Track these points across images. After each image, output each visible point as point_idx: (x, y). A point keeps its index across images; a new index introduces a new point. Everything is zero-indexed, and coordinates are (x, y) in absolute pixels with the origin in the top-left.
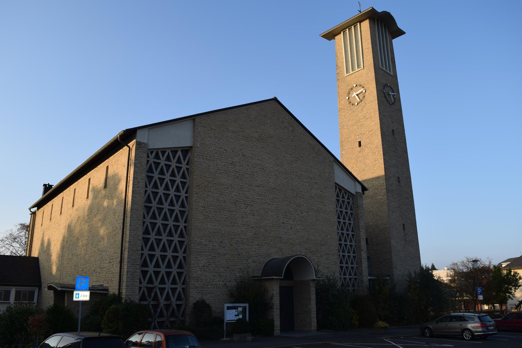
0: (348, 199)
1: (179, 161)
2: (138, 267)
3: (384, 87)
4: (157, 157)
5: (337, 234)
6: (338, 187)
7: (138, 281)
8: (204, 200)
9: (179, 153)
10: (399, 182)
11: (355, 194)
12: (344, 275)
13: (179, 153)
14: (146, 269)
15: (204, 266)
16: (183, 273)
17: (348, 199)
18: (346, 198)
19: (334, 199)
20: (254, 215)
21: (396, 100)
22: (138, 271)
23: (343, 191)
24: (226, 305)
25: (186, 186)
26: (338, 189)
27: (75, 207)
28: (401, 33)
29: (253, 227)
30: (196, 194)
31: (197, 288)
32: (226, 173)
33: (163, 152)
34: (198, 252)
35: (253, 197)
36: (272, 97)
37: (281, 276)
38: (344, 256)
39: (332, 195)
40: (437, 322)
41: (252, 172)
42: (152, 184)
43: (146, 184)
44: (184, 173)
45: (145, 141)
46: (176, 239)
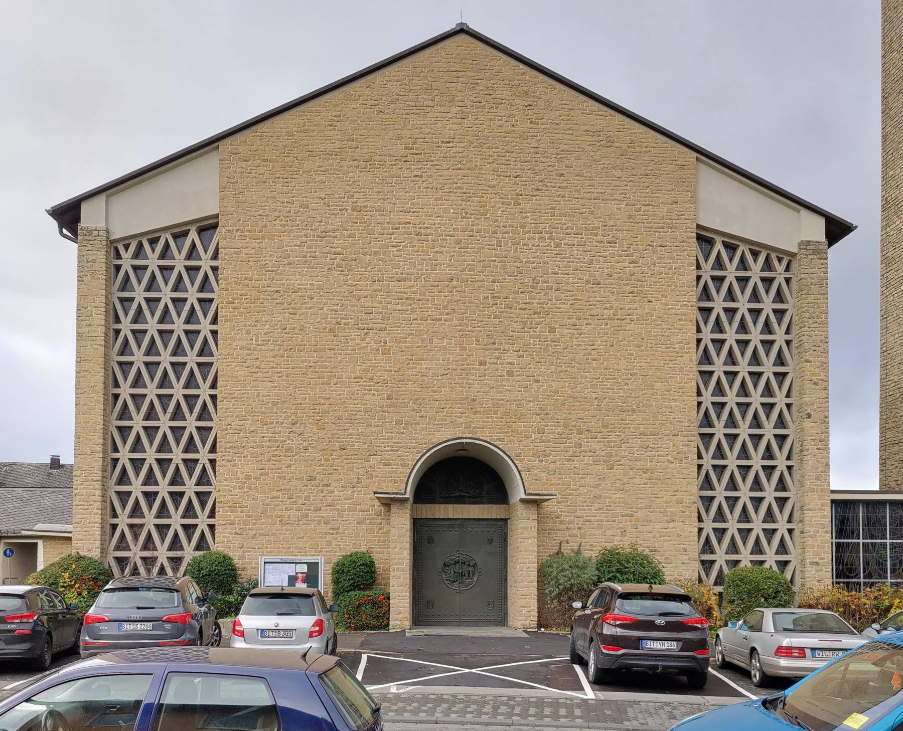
8: (248, 333)
9: (193, 235)
13: (193, 235)
14: (709, 493)
15: (248, 477)
20: (386, 352)
23: (743, 248)
29: (385, 382)
30: (226, 321)
39: (682, 264)
42: (711, 323)
46: (191, 423)
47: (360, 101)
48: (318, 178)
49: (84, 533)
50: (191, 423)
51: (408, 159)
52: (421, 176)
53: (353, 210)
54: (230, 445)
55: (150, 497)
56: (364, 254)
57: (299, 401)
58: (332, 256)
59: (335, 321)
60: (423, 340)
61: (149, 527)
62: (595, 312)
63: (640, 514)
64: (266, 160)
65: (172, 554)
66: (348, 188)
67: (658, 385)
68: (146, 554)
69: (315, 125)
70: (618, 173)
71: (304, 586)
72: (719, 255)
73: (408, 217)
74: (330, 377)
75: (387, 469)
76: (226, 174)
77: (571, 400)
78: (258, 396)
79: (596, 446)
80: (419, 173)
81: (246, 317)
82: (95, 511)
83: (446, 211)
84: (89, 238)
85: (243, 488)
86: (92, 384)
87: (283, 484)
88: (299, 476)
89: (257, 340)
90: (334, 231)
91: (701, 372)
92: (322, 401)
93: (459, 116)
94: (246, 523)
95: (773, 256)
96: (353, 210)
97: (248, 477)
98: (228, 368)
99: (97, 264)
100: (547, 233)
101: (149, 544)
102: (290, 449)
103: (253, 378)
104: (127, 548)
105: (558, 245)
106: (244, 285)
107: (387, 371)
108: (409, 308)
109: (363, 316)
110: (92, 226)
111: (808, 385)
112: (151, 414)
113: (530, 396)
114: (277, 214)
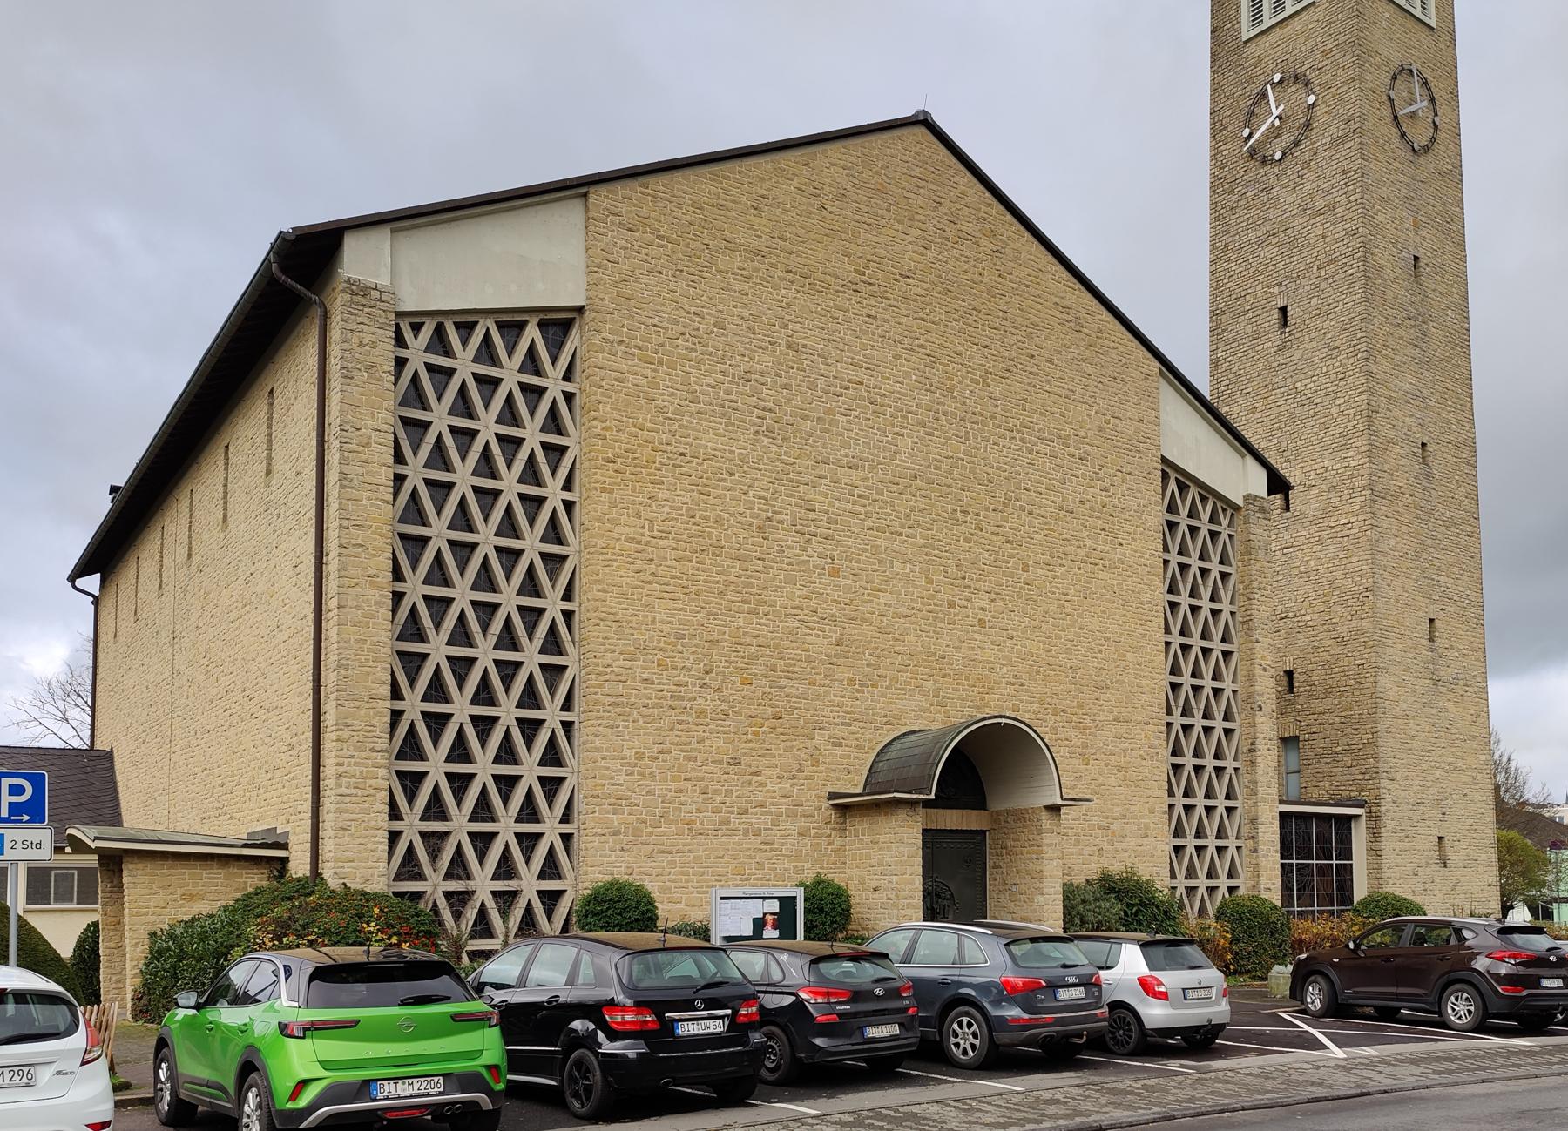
0: (1213, 519)
1: (532, 363)
2: (381, 759)
3: (1394, 78)
4: (440, 343)
5: (1162, 647)
6: (1173, 475)
7: (386, 808)
9: (532, 333)
10: (1425, 462)
11: (1240, 502)
12: (1186, 795)
13: (532, 333)
15: (640, 756)
16: (561, 780)
17: (1211, 521)
18: (1205, 516)
19: (1158, 517)
20: (834, 573)
21: (1442, 135)
22: (382, 772)
23: (1193, 490)
25: (566, 463)
26: (1172, 485)
30: (603, 490)
31: (616, 833)
33: (466, 328)
36: (907, 112)
41: (828, 411)
43: (396, 441)
44: (553, 410)
45: (384, 281)
47: (795, 183)
49: (356, 848)
50: (531, 657)
51: (858, 287)
52: (875, 318)
53: (789, 347)
54: (611, 699)
55: (460, 783)
56: (805, 418)
57: (715, 636)
58: (761, 413)
59: (764, 515)
60: (880, 561)
61: (459, 837)
62: (1068, 549)
63: (1115, 826)
64: (660, 237)
65: (501, 886)
66: (780, 312)
67: (1130, 656)
68: (454, 886)
69: (734, 202)
70: (1088, 369)
71: (776, 934)
72: (532, 349)
73: (859, 375)
74: (759, 603)
75: (839, 751)
76: (601, 245)
77: (1045, 667)
78: (653, 622)
79: (1072, 733)
80: (873, 313)
81: (633, 489)
82: (378, 807)
83: (907, 376)
84: (364, 301)
85: (632, 774)
86: (371, 572)
87: (694, 770)
88: (718, 757)
89: (651, 529)
90: (763, 374)
91: (403, 537)
92: (748, 640)
93: (921, 242)
95: (1219, 505)
96: (789, 347)
97: (640, 756)
98: (607, 570)
100: (1019, 432)
101: (458, 867)
102: (702, 713)
103: (645, 592)
104: (420, 876)
105: (1030, 452)
106: (631, 434)
107: (834, 601)
108: (863, 510)
109: (803, 513)
110: (368, 279)
111: (1259, 671)
112: (461, 635)
113: (1004, 658)
114: (680, 328)
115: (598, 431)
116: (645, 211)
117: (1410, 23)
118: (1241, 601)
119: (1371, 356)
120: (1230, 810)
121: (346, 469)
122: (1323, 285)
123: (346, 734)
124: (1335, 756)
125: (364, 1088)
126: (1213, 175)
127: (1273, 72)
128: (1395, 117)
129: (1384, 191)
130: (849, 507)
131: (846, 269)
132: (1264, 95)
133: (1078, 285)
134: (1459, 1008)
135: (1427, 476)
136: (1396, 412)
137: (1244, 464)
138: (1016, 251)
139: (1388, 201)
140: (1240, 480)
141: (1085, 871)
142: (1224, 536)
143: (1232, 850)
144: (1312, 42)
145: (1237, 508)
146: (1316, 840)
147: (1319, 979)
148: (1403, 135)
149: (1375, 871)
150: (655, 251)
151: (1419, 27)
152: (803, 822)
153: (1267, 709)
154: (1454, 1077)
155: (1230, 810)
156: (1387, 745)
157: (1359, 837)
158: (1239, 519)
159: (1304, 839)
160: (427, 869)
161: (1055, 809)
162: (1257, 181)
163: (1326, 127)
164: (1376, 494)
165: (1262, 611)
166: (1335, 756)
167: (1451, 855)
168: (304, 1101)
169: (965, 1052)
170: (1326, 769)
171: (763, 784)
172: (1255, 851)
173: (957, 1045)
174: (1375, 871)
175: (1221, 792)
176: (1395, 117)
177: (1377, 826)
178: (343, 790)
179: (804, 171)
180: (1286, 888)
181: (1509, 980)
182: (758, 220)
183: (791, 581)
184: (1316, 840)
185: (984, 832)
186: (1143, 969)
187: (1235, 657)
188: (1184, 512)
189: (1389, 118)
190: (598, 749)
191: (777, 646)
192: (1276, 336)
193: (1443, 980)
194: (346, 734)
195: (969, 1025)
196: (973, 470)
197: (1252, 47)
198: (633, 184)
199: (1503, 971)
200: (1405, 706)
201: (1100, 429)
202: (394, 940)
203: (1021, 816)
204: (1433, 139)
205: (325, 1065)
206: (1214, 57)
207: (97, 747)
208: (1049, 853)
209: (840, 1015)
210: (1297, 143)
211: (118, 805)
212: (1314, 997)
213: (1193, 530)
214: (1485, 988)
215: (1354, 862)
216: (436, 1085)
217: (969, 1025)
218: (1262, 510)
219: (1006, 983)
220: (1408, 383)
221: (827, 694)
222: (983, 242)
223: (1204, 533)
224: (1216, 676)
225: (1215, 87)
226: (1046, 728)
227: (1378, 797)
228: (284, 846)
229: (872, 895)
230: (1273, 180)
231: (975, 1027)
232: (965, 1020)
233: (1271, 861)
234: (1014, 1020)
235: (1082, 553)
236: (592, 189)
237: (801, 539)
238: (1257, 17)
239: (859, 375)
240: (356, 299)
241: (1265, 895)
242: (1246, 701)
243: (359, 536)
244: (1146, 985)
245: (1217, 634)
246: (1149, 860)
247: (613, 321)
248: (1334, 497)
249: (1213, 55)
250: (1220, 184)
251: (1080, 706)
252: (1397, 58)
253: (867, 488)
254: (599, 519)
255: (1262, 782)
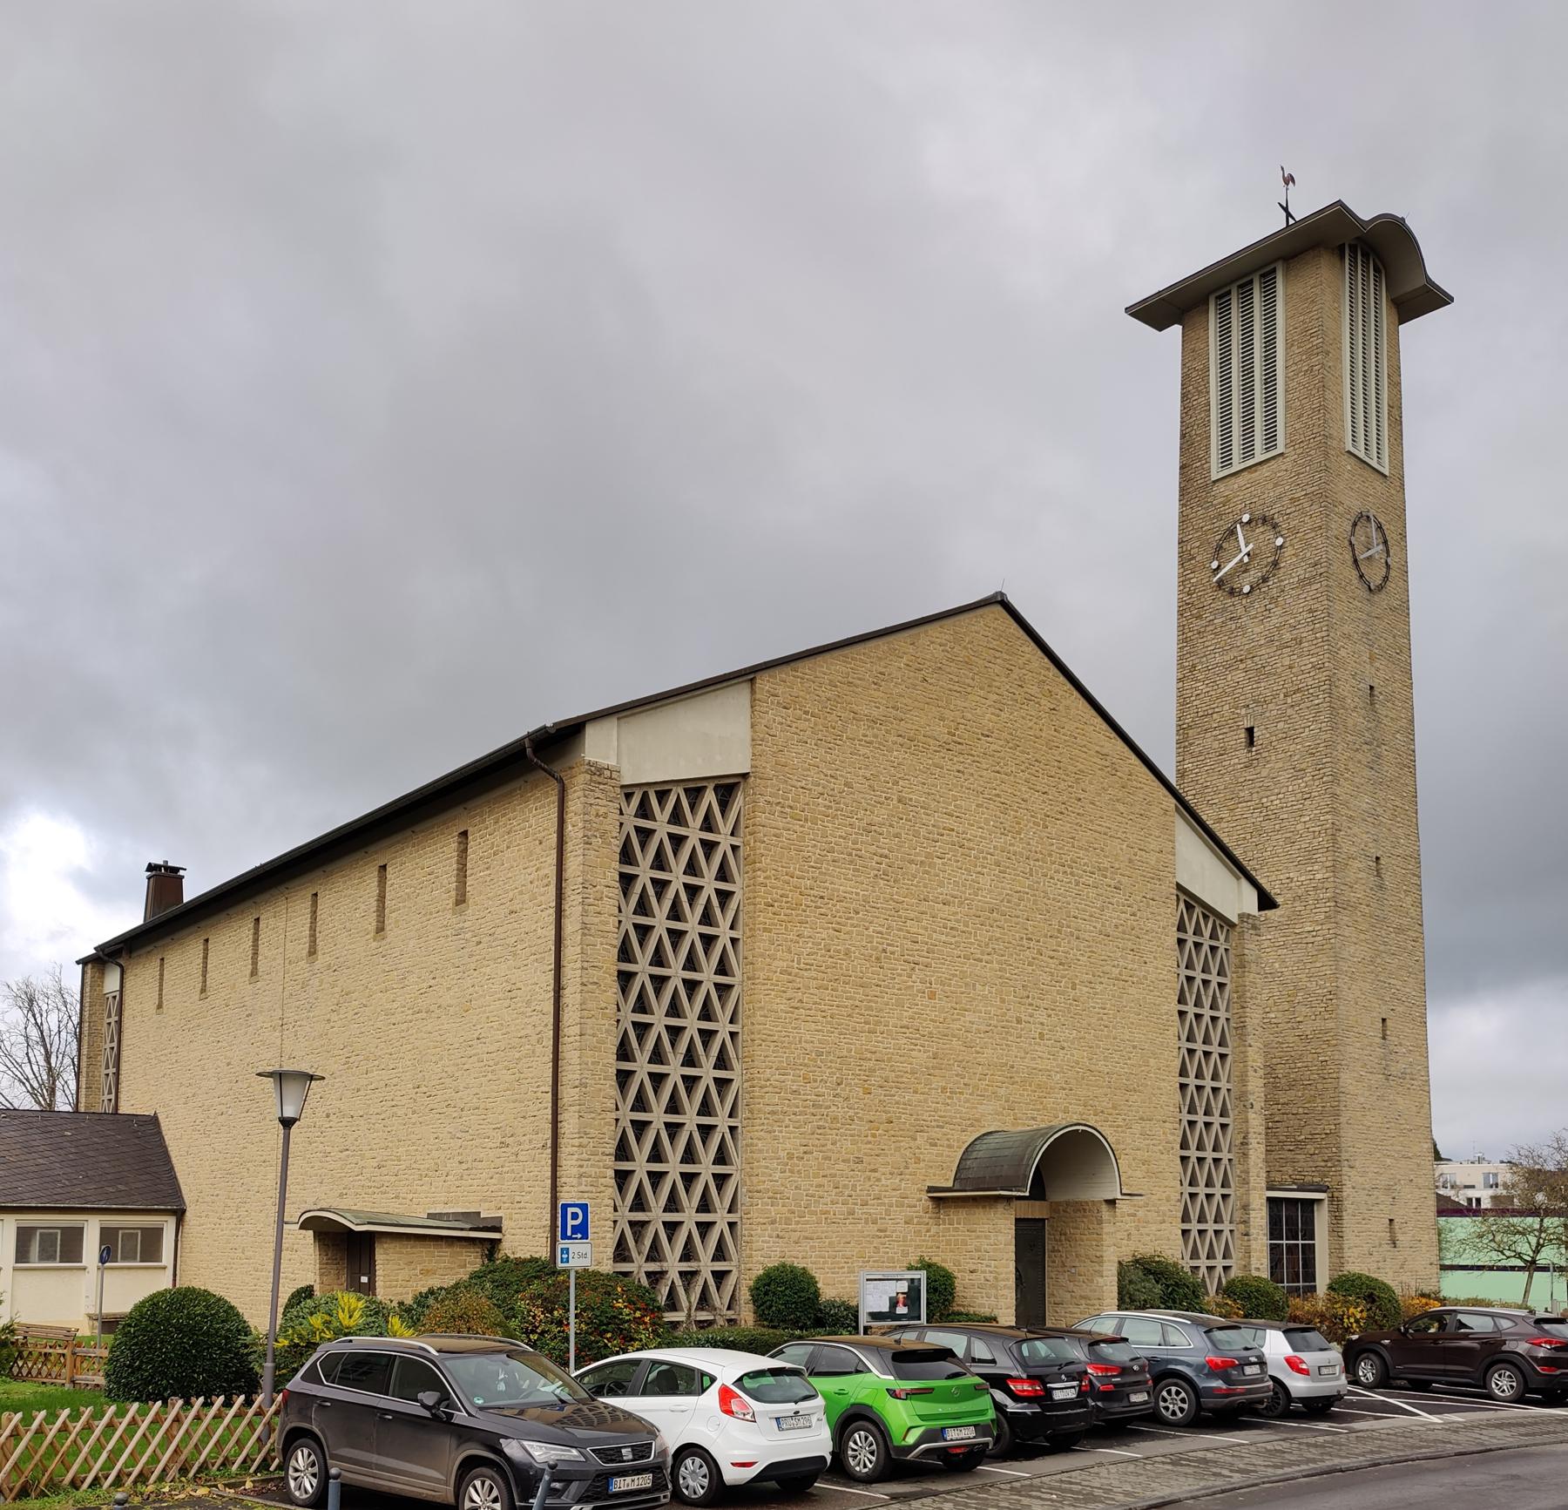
0: (1214, 936)
1: (708, 825)
3: (1355, 525)
4: (644, 811)
6: (1182, 897)
9: (710, 797)
10: (1379, 875)
11: (1235, 920)
13: (710, 797)
18: (1207, 933)
20: (932, 996)
21: (1393, 573)
24: (864, 1275)
25: (733, 905)
26: (1182, 905)
27: (321, 960)
28: (1433, 299)
30: (765, 930)
31: (773, 1223)
32: (851, 862)
33: (662, 796)
34: (773, 1113)
35: (930, 937)
37: (1023, 1186)
38: (1191, 1124)
40: (993, 1361)
41: (928, 856)
45: (612, 762)
48: (863, 751)
54: (770, 1108)
57: (845, 1053)
64: (806, 713)
65: (685, 1267)
70: (1121, 807)
73: (951, 823)
74: (878, 1023)
75: (935, 1150)
83: (987, 822)
90: (881, 825)
94: (788, 1221)
99: (609, 820)
102: (835, 1119)
109: (909, 945)
110: (604, 762)
111: (1251, 1073)
114: (820, 789)
115: (761, 880)
116: (795, 692)
117: (1367, 473)
118: (1235, 1009)
119: (1335, 780)
120: (1224, 1197)
121: (586, 920)
122: (1290, 711)
123: (585, 1141)
124: (1299, 1144)
125: (938, 1434)
126: (1180, 600)
127: (1242, 512)
128: (1356, 561)
129: (1346, 629)
130: (943, 938)
131: (940, 731)
132: (1233, 532)
133: (1113, 735)
134: (1502, 1383)
135: (1381, 887)
136: (1356, 830)
137: (1240, 892)
138: (1067, 708)
139: (1349, 637)
140: (1235, 900)
141: (1126, 1252)
142: (1221, 951)
143: (1226, 1233)
144: (1279, 490)
145: (1232, 925)
146: (1291, 1219)
147: (1372, 1356)
148: (1361, 576)
149: (1337, 1251)
150: (803, 725)
151: (1376, 476)
152: (909, 1212)
153: (1257, 1106)
154: (1538, 1439)
155: (1224, 1197)
156: (1348, 1135)
157: (1322, 1219)
158: (1234, 935)
159: (1292, 1221)
160: (634, 1254)
161: (1112, 1203)
162: (1224, 610)
163: (1293, 569)
164: (1338, 904)
165: (1254, 1018)
166: (1299, 1144)
167: (1400, 1237)
168: (911, 1440)
169: (1174, 1413)
170: (1290, 1155)
171: (879, 1180)
172: (1247, 1235)
173: (1167, 1408)
174: (1337, 1251)
175: (1218, 1181)
176: (1356, 561)
177: (1339, 1210)
178: (583, 1188)
179: (911, 649)
180: (1275, 1264)
181: (1544, 1361)
182: (876, 694)
183: (900, 1004)
184: (1291, 1219)
185: (1043, 1220)
186: (1288, 1351)
187: (1229, 1059)
188: (1191, 930)
189: (1350, 562)
190: (761, 1151)
191: (889, 1060)
192: (1243, 754)
193: (1489, 1360)
194: (585, 1141)
195: (1178, 1393)
196: (1035, 902)
197: (1221, 487)
198: (787, 669)
199: (1541, 1355)
200: (1362, 1100)
201: (1130, 861)
202: (638, 1314)
203: (1081, 1208)
204: (1386, 579)
205: (922, 1417)
206: (1183, 491)
207: (125, 1109)
208: (1107, 1240)
209: (1116, 1385)
210: (1265, 580)
211: (172, 1168)
212: (1366, 1372)
213: (1197, 945)
214: (1525, 1367)
215: (1317, 1242)
216: (971, 1432)
217: (1178, 1393)
218: (1254, 927)
219: (1210, 1362)
220: (1364, 802)
221: (926, 1101)
222: (1043, 702)
223: (1206, 948)
224: (1215, 1077)
225: (1184, 520)
226: (1109, 1133)
227: (1340, 1183)
228: (498, 1229)
229: (967, 1276)
230: (1241, 611)
231: (1183, 1395)
232: (1174, 1389)
233: (1260, 1242)
234: (1219, 1389)
235: (1116, 971)
236: (758, 675)
237: (908, 967)
238: (1226, 460)
239: (951, 823)
240: (595, 778)
241: (1255, 1274)
242: (1239, 1099)
243: (595, 975)
244: (1293, 1364)
245: (1216, 1039)
246: (1170, 1247)
247: (773, 786)
248: (1299, 906)
249: (1182, 489)
250: (1187, 610)
251: (1114, 1108)
252: (1355, 504)
253: (958, 921)
254: (762, 955)
255: (1253, 1172)
